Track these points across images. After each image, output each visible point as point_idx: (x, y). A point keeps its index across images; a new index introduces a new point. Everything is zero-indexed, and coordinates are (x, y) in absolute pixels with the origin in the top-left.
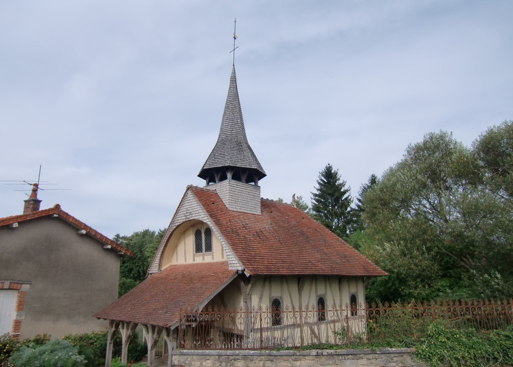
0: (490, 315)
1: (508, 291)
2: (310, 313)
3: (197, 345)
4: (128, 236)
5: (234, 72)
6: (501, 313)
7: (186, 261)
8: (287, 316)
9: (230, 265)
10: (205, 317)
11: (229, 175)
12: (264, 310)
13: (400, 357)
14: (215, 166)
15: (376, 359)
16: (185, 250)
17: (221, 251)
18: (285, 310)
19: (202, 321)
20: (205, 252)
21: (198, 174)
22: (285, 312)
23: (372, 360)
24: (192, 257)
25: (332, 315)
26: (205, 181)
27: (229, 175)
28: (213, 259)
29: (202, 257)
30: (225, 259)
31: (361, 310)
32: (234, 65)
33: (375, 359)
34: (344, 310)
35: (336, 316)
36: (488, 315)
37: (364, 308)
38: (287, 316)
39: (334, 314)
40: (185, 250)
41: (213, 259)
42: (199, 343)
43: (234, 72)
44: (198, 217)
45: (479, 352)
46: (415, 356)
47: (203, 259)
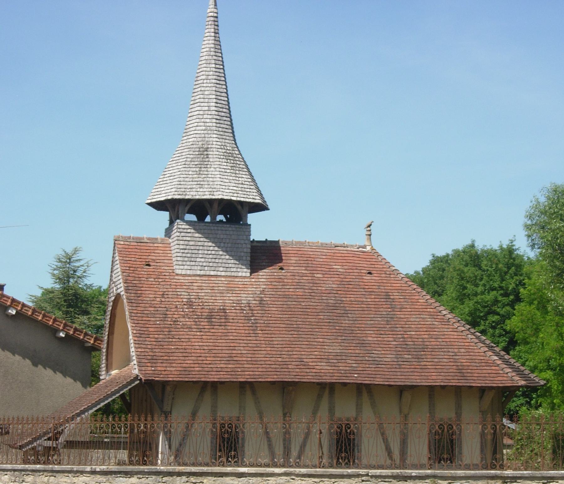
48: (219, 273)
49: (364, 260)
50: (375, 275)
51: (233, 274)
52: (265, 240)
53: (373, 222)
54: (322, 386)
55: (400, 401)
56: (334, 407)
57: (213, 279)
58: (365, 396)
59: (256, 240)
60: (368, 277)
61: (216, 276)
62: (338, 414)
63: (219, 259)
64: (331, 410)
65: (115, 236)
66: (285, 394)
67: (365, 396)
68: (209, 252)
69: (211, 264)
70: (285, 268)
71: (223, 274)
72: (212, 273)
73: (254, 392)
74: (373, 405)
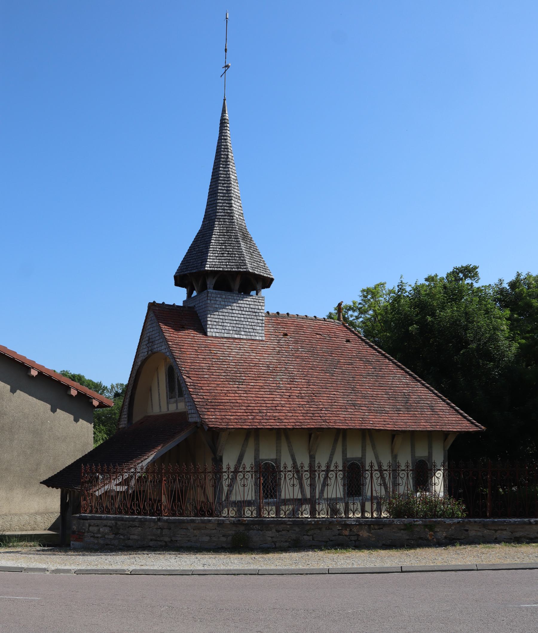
1: (49, 446)
2: (403, 472)
4: (85, 378)
8: (285, 478)
9: (190, 416)
12: (289, 469)
13: (316, 530)
14: (262, 274)
15: (288, 531)
18: (282, 469)
22: (282, 471)
23: (283, 532)
25: (290, 477)
26: (186, 289)
31: (399, 470)
33: (287, 531)
34: (368, 470)
35: (296, 478)
37: (411, 469)
38: (285, 478)
39: (293, 476)
48: (242, 337)
49: (341, 331)
50: (353, 343)
51: (253, 338)
52: (172, 304)
53: (342, 302)
54: (339, 431)
55: (392, 443)
56: (346, 449)
57: (237, 341)
58: (283, 438)
59: (166, 303)
60: (348, 344)
61: (240, 339)
62: (349, 456)
63: (242, 324)
64: (257, 452)
65: (174, 304)
66: (312, 439)
67: (283, 438)
68: (234, 318)
69: (235, 329)
70: (289, 334)
71: (245, 337)
72: (236, 336)
73: (287, 438)
74: (374, 447)
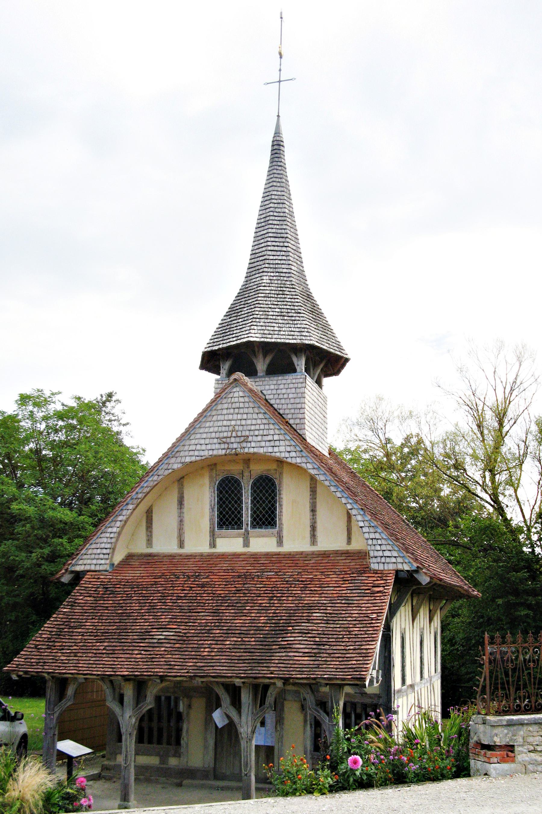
0: (534, 661)
3: (523, 705)
5: (277, 133)
6: (510, 658)
7: (181, 544)
10: (534, 652)
11: (301, 363)
16: (181, 522)
17: (309, 529)
19: (529, 661)
20: (254, 526)
21: (348, 364)
24: (208, 538)
27: (301, 363)
28: (280, 542)
29: (241, 540)
30: (357, 545)
32: (278, 116)
36: (529, 661)
40: (181, 522)
41: (280, 542)
42: (526, 703)
43: (277, 133)
44: (270, 450)
45: (328, 756)
46: (525, 735)
47: (246, 544)
